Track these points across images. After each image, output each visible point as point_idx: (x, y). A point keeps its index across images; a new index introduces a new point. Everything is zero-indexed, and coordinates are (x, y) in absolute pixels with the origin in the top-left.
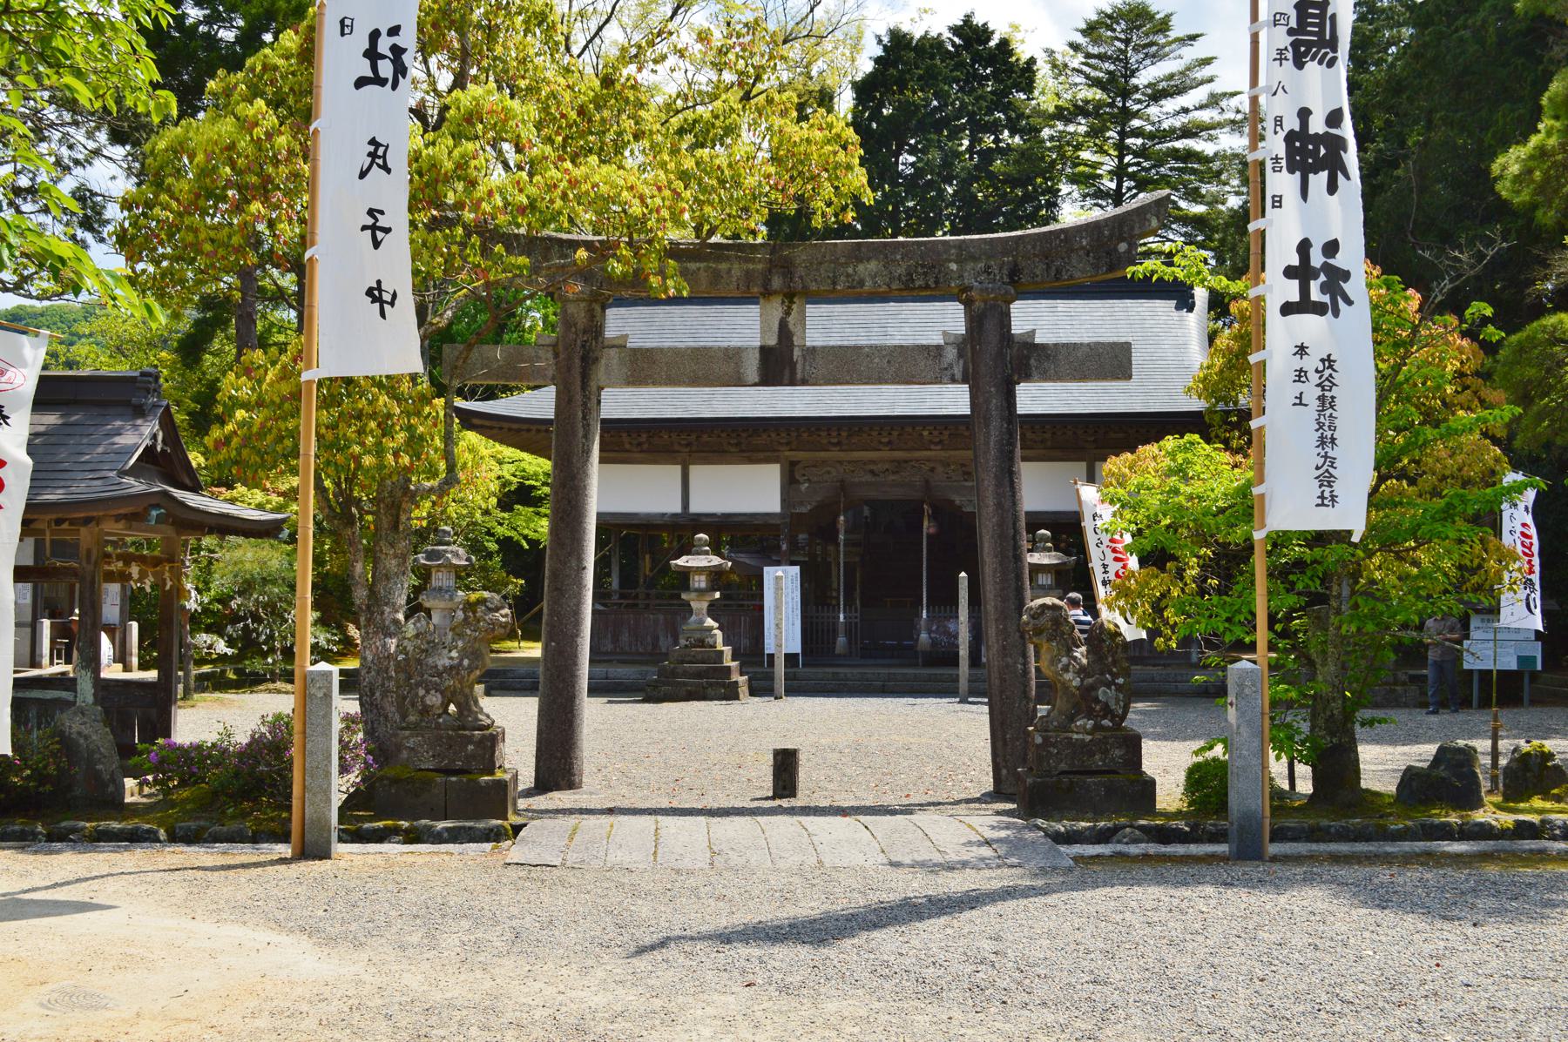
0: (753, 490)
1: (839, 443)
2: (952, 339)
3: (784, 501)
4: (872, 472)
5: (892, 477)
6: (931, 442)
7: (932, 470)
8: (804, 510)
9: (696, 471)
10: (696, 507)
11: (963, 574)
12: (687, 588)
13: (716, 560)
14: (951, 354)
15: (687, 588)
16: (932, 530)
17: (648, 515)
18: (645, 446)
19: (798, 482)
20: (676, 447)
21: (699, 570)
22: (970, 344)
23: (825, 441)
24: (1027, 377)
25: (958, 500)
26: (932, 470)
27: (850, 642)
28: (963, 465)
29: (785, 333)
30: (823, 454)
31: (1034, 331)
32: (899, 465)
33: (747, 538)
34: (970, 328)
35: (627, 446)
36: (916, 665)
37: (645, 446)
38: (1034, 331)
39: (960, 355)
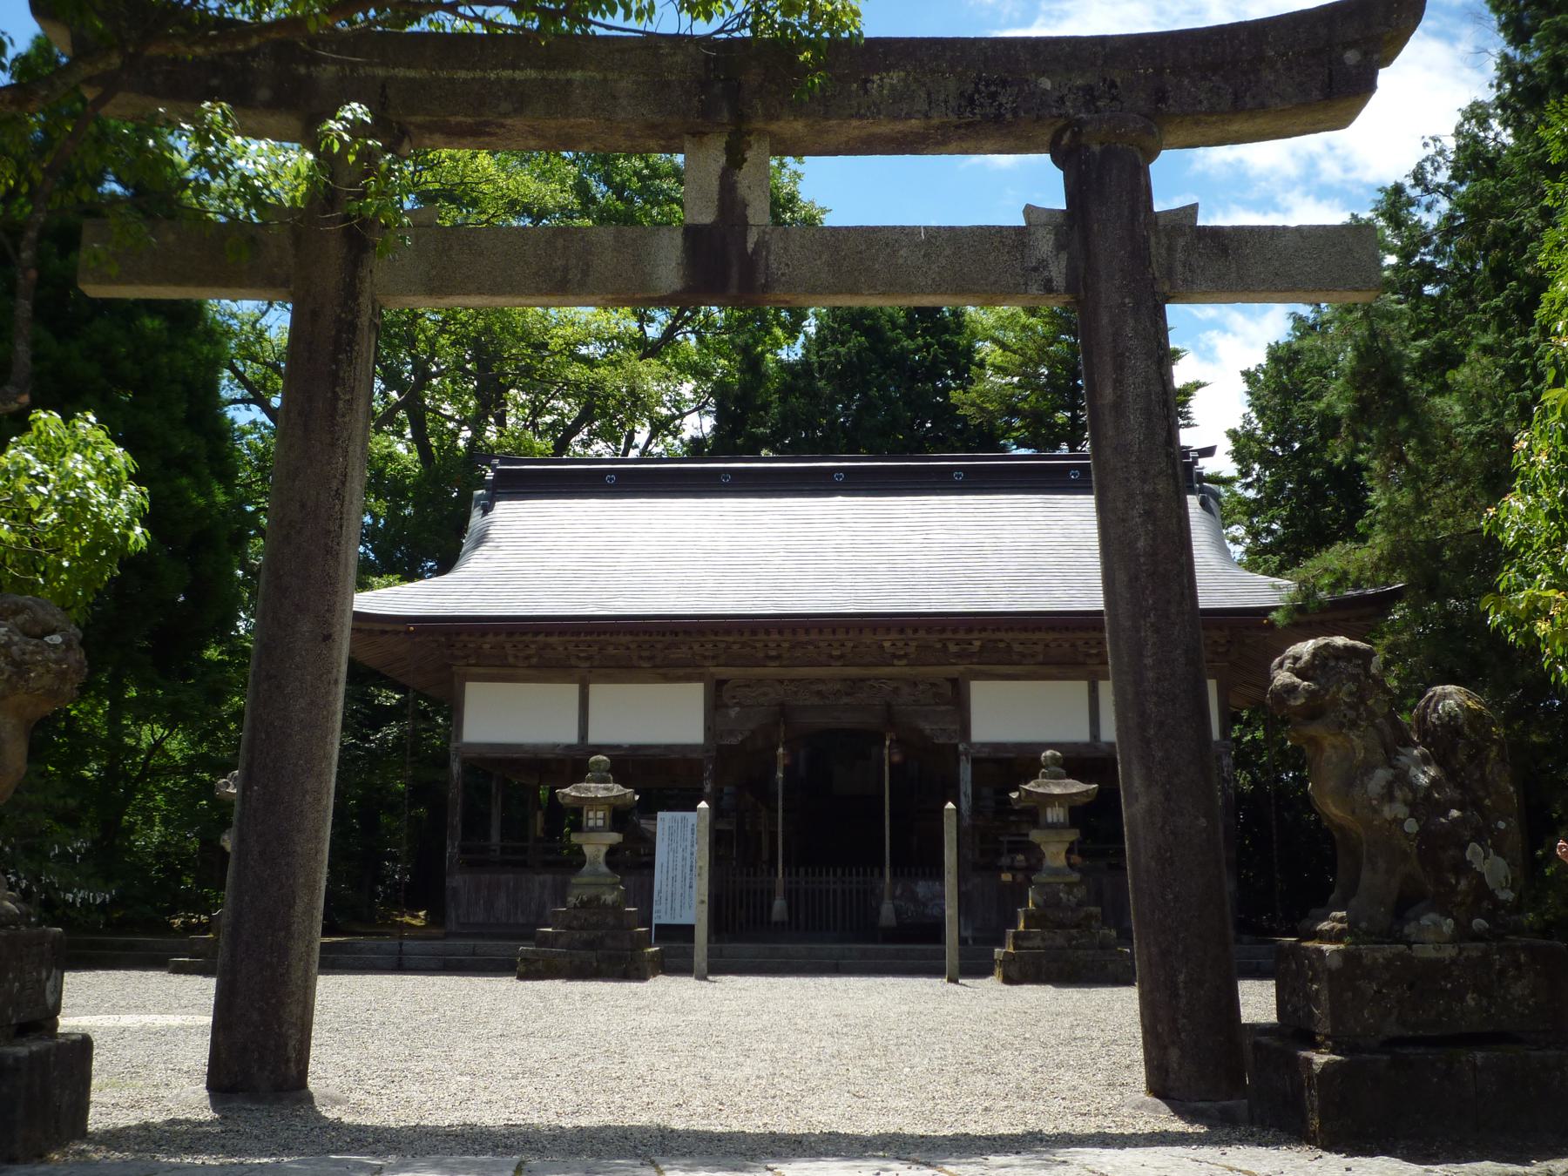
0: (669, 715)
1: (778, 657)
2: (1044, 219)
3: (708, 729)
4: (819, 693)
5: (845, 700)
6: (894, 656)
7: (896, 690)
8: (734, 741)
9: (595, 690)
10: (594, 738)
11: (950, 805)
12: (578, 827)
13: (617, 790)
14: (1045, 244)
15: (578, 827)
16: (896, 758)
17: (536, 747)
18: (534, 661)
19: (726, 706)
20: (573, 661)
21: (594, 802)
22: (1075, 222)
23: (761, 655)
24: (1168, 302)
25: (927, 727)
26: (896, 690)
27: (789, 907)
28: (933, 685)
29: (730, 202)
30: (758, 671)
31: (1193, 208)
32: (855, 684)
33: (657, 777)
34: (1074, 191)
35: (511, 660)
36: (875, 941)
37: (534, 661)
38: (1193, 208)
39: (1060, 246)
